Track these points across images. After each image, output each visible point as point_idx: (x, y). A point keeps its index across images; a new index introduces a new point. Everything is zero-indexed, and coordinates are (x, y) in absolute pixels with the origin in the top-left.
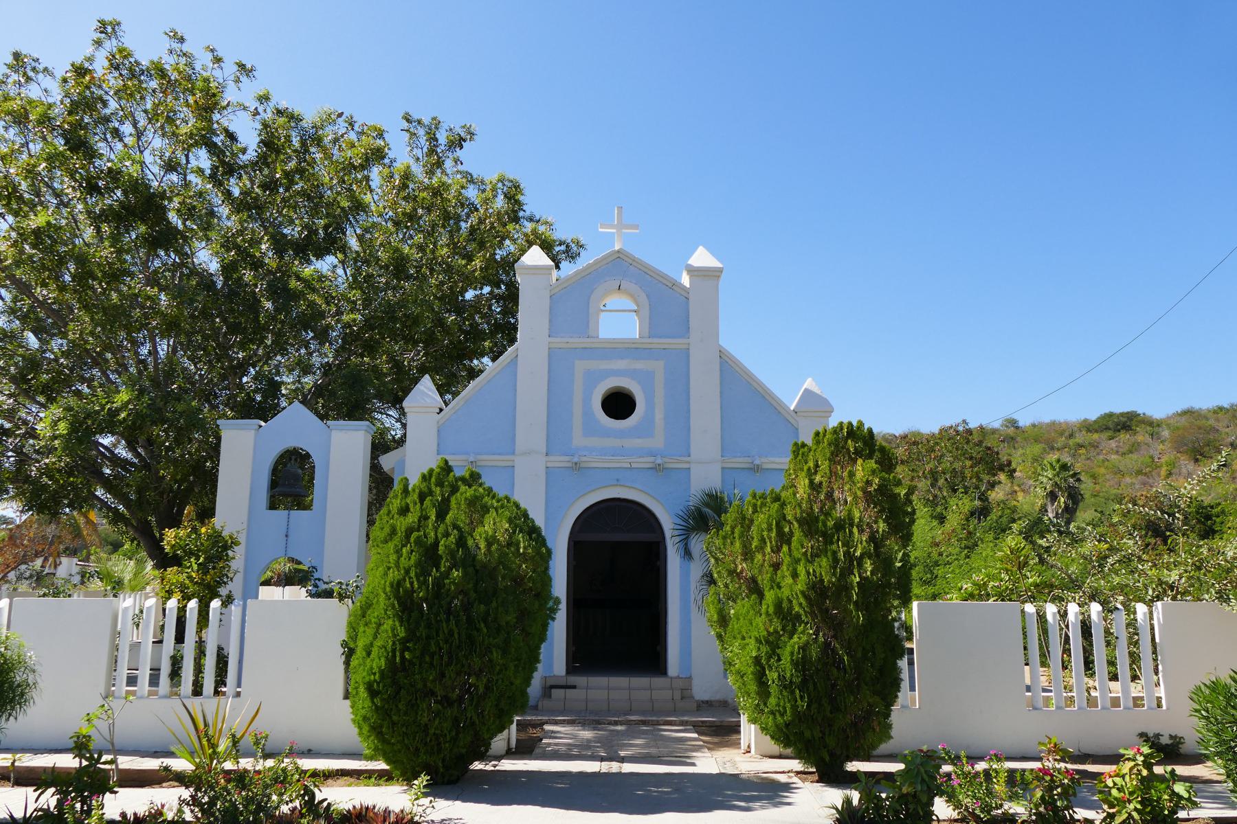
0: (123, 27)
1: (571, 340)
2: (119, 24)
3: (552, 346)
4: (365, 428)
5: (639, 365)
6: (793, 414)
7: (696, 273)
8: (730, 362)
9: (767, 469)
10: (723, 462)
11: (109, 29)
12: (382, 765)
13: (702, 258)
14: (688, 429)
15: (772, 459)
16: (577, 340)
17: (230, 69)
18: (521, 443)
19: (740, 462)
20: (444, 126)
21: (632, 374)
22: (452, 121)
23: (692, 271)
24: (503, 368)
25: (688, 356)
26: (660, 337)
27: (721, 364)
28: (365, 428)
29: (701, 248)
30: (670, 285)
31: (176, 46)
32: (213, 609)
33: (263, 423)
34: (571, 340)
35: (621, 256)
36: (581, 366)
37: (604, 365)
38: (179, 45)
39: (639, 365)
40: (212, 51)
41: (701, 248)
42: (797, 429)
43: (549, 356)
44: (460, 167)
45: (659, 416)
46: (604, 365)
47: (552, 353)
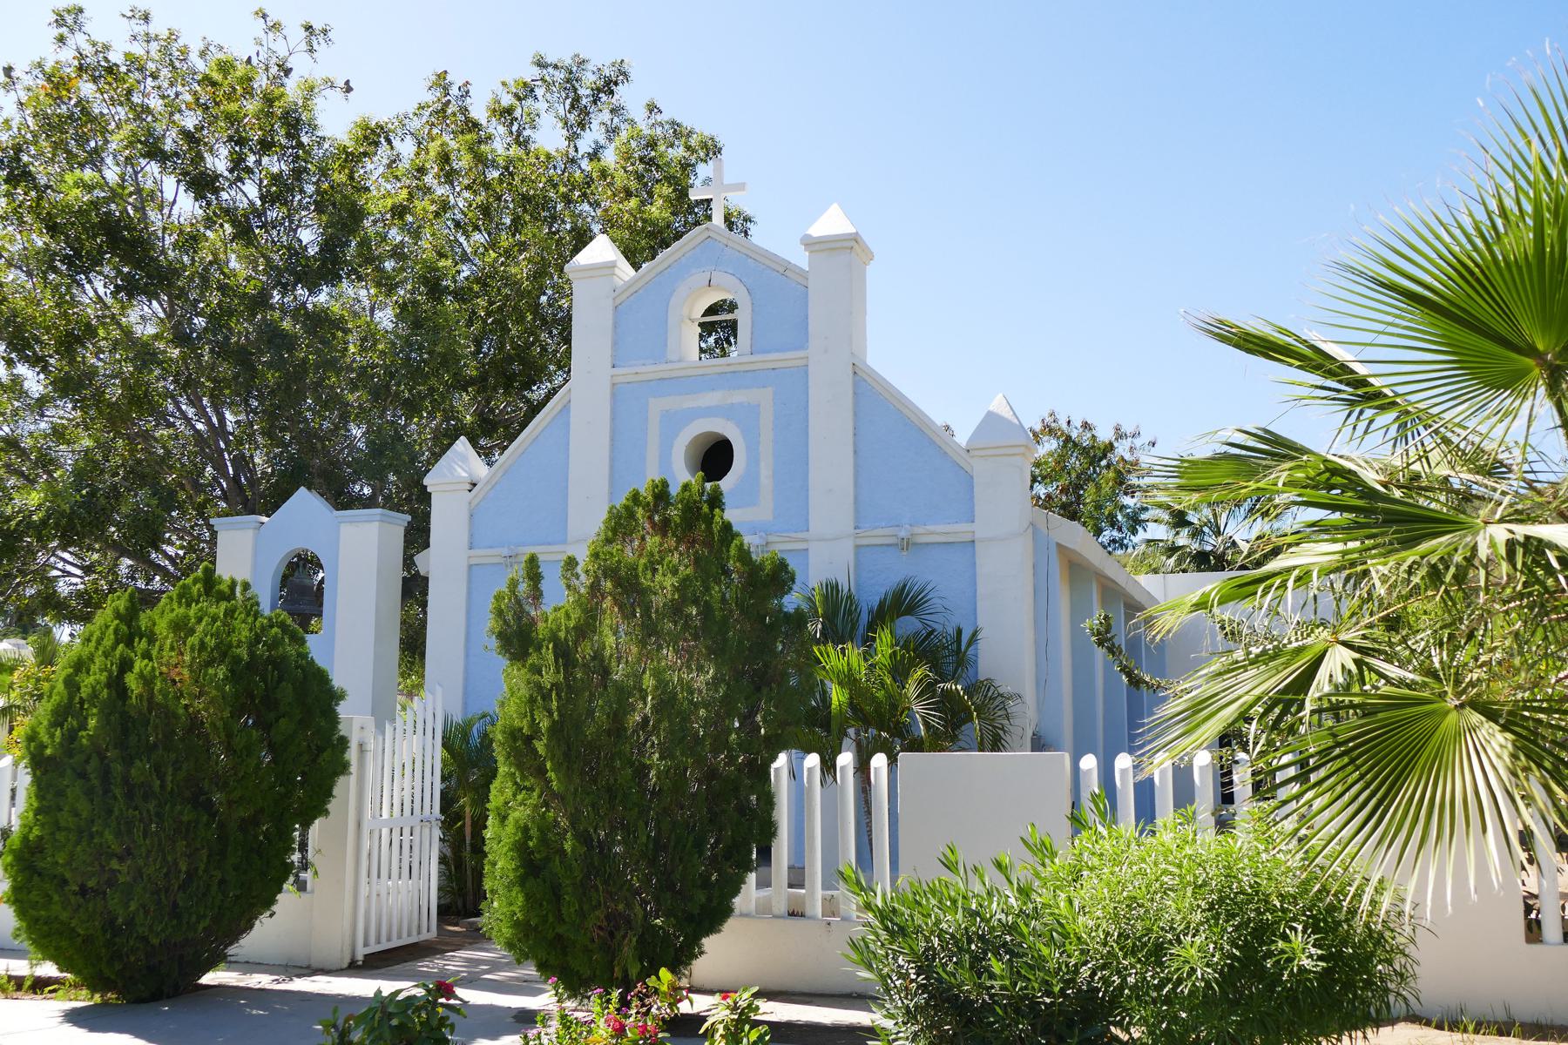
0: (86, 14)
1: (643, 369)
2: (81, 11)
3: (617, 380)
4: (378, 517)
5: (738, 397)
6: (964, 454)
7: (817, 247)
8: (869, 380)
9: (927, 544)
10: (857, 536)
11: (69, 19)
12: (49, 969)
13: (832, 223)
14: (805, 488)
15: (931, 528)
16: (653, 368)
17: (297, 36)
18: (817, 524)
19: (879, 535)
20: (590, 67)
21: (727, 412)
22: (601, 59)
23: (811, 244)
24: (553, 419)
25: (806, 373)
26: (769, 352)
27: (856, 385)
28: (378, 517)
29: (835, 206)
30: (781, 270)
31: (141, 29)
32: (1201, 768)
33: (264, 519)
34: (643, 369)
35: (712, 234)
36: (763, 397)
37: (689, 403)
38: (145, 27)
39: (738, 397)
40: (264, 16)
41: (835, 206)
42: (972, 477)
43: (614, 395)
44: (659, 118)
45: (765, 473)
46: (689, 403)
47: (616, 391)
